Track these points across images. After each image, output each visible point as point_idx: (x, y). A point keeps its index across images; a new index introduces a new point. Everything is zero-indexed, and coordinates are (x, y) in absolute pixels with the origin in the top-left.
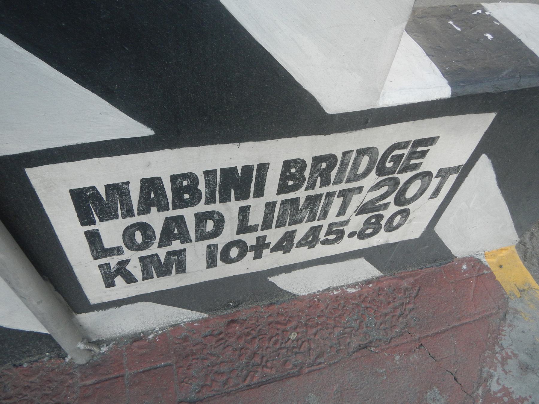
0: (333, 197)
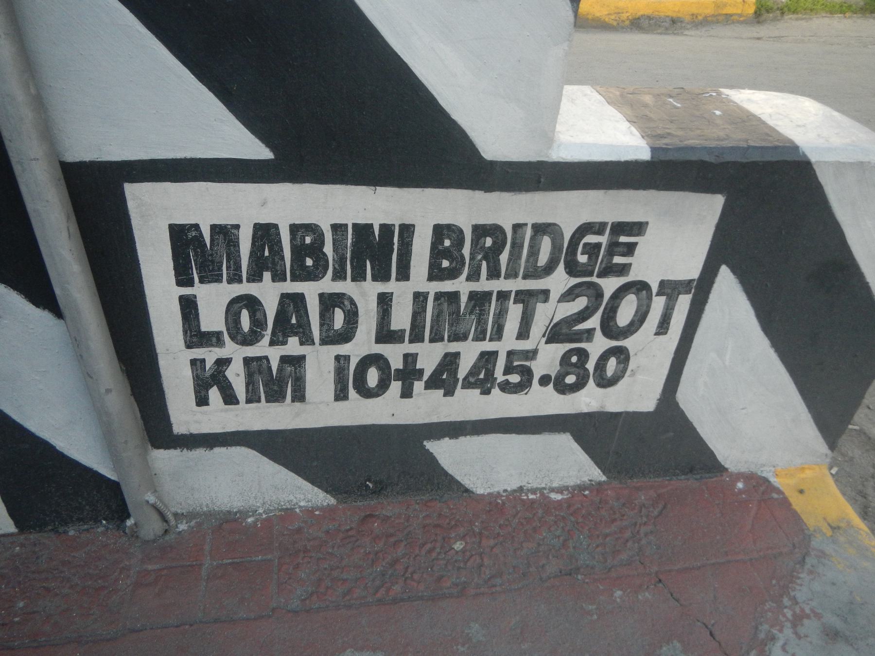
0: (507, 301)
